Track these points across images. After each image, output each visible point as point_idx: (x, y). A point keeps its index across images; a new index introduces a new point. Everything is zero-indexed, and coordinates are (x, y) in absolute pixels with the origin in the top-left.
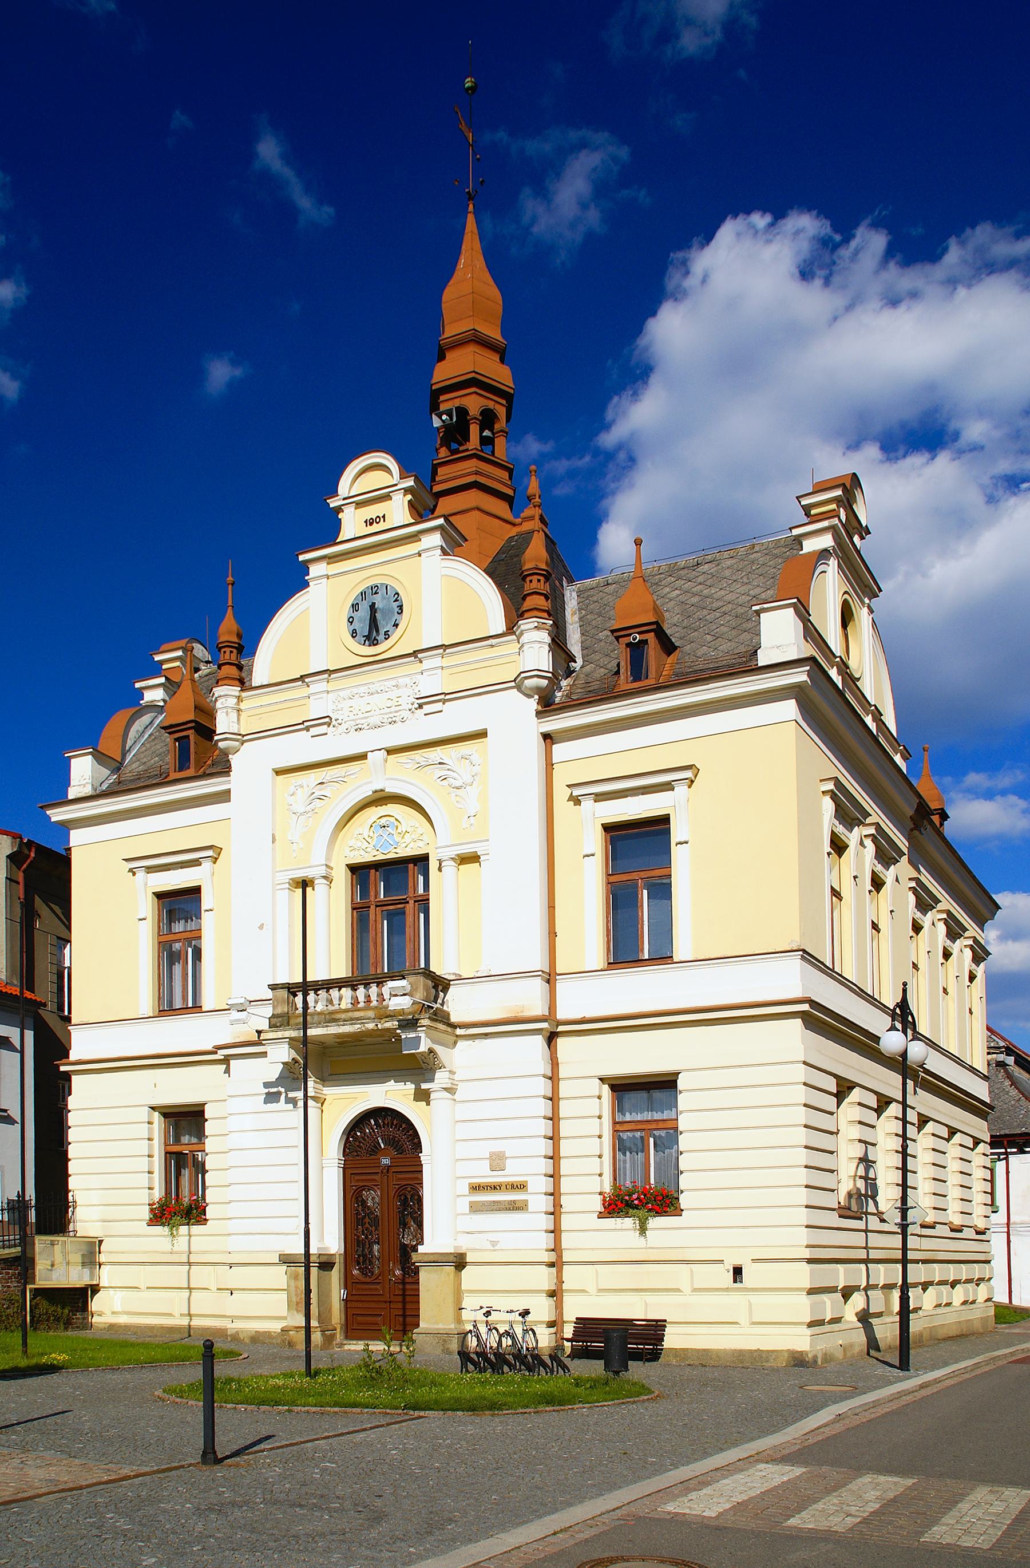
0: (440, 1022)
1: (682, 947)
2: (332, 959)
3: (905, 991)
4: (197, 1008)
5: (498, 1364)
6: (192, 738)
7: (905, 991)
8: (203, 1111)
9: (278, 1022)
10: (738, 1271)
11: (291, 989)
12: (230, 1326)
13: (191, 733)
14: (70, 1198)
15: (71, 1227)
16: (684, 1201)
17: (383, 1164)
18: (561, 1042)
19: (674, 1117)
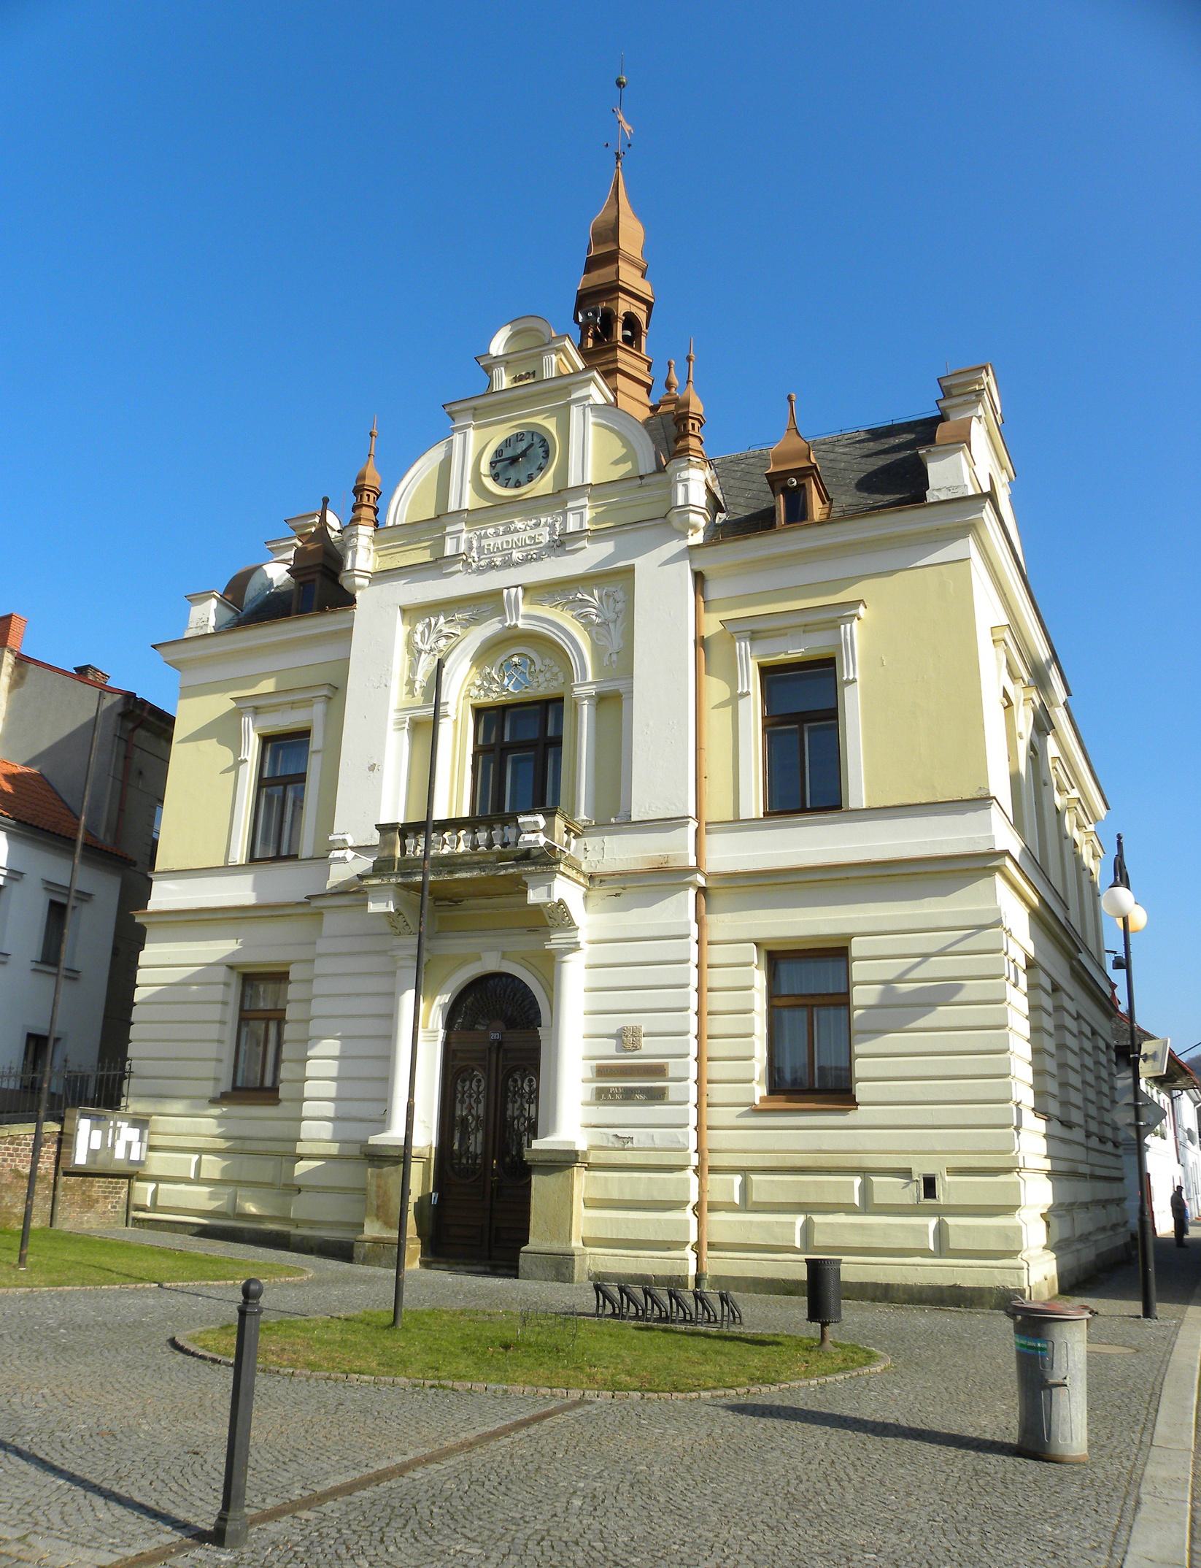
0: (573, 868)
1: (858, 791)
2: (454, 795)
3: (1119, 844)
4: (293, 857)
5: (650, 1306)
6: (317, 584)
7: (1119, 844)
8: (288, 973)
9: (381, 868)
10: (930, 1185)
11: (407, 830)
12: (294, 1231)
13: (317, 577)
14: (127, 1067)
15: (537, 1241)
16: (862, 1091)
17: (499, 1037)
18: (212, 1083)
19: (843, 990)
